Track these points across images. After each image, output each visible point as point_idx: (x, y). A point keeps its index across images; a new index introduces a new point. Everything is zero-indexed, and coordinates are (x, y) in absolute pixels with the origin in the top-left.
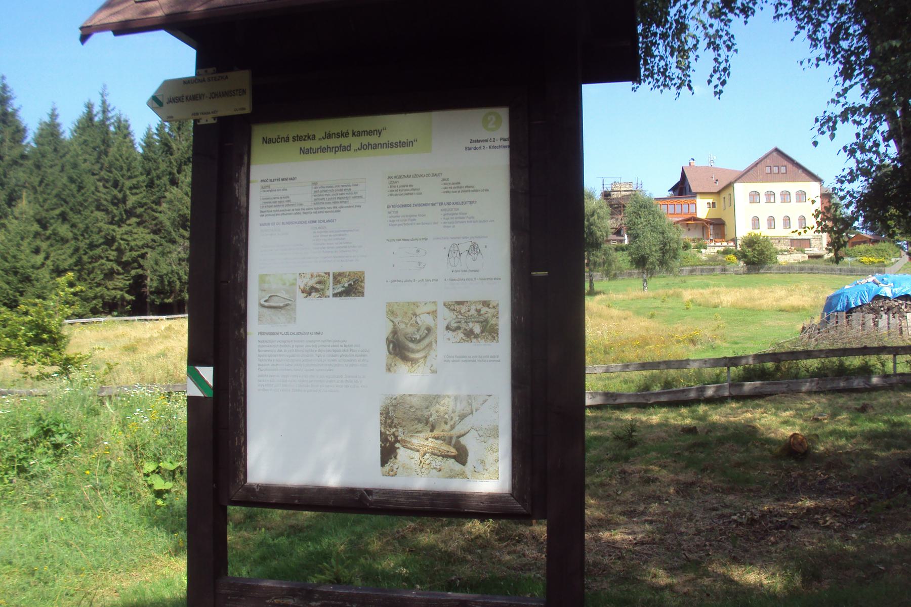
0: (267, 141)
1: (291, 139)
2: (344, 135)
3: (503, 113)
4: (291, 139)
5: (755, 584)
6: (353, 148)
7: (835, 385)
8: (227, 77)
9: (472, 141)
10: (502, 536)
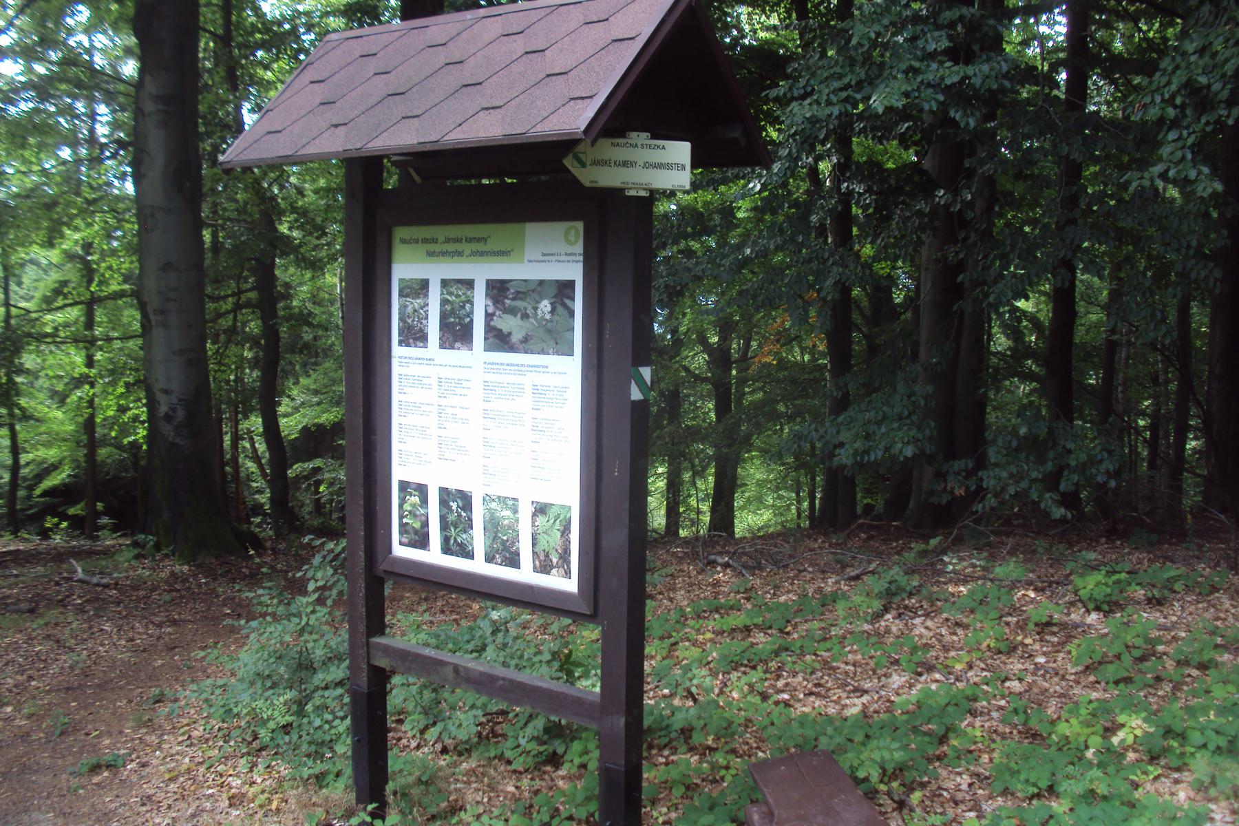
0: (403, 241)
3: (580, 225)
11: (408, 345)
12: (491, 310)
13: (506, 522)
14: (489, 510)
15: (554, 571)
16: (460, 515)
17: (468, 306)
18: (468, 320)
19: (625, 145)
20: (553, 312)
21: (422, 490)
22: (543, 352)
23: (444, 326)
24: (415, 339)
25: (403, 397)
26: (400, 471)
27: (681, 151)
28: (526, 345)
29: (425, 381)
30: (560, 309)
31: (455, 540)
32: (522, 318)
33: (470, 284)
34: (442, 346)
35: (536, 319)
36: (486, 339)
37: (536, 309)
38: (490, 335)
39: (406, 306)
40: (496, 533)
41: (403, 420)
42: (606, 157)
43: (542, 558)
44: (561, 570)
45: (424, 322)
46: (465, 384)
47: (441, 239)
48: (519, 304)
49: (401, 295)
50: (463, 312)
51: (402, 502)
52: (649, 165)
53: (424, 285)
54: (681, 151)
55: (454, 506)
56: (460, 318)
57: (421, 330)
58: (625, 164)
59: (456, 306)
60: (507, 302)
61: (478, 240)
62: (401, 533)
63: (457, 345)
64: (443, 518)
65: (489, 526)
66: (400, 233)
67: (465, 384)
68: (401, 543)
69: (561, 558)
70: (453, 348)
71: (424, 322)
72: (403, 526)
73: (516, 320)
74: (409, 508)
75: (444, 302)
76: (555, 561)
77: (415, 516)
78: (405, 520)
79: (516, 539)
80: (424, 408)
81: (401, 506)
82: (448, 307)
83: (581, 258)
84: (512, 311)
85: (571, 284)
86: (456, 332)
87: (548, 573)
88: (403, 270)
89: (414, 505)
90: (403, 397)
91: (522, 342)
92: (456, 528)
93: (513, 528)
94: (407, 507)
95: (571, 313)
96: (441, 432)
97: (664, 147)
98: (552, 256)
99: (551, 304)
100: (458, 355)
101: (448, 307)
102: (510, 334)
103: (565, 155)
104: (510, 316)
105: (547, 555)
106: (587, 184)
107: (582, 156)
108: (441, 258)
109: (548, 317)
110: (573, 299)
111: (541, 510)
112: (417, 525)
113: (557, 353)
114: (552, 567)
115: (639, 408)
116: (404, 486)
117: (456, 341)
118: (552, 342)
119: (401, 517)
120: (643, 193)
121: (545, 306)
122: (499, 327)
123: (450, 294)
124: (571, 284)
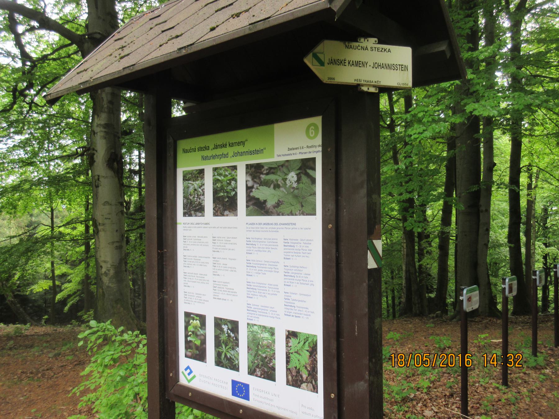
0: (185, 151)
1: (197, 150)
2: (224, 146)
3: (318, 121)
4: (197, 150)
5: (415, 318)
6: (210, 149)
7: (509, 303)
8: (355, 80)
9: (290, 149)
10: (136, 164)
11: (190, 215)
12: (250, 184)
13: (265, 342)
14: (252, 332)
15: (304, 385)
16: (229, 336)
17: (233, 183)
18: (234, 193)
19: (357, 48)
20: (299, 180)
21: (202, 318)
22: (291, 214)
23: (216, 199)
24: (196, 211)
25: (186, 253)
26: (184, 306)
27: (403, 55)
28: (277, 209)
29: (203, 240)
30: (304, 178)
31: (226, 355)
32: (274, 188)
33: (235, 168)
34: (215, 215)
35: (285, 188)
36: (247, 206)
37: (285, 180)
38: (251, 203)
39: (188, 187)
40: (257, 351)
41: (187, 270)
42: (342, 58)
43: (294, 374)
44: (310, 385)
45: (201, 197)
46: (233, 241)
47: (212, 147)
48: (272, 177)
49: (185, 179)
50: (230, 187)
51: (187, 324)
52: (377, 66)
53: (202, 172)
54: (403, 55)
55: (225, 328)
56: (227, 192)
57: (200, 204)
58: (358, 64)
59: (225, 183)
60: (263, 177)
61: (239, 144)
62: (186, 348)
63: (226, 212)
64: (217, 337)
65: (252, 346)
66: (183, 144)
67: (233, 241)
68: (186, 356)
69: (309, 375)
70: (223, 215)
71: (201, 197)
72: (187, 343)
73: (270, 193)
74: (192, 329)
75: (216, 181)
76: (305, 376)
77: (197, 335)
78: (189, 339)
79: (272, 357)
80: (203, 260)
81: (186, 328)
82: (219, 185)
83: (320, 149)
84: (266, 184)
85: (314, 159)
86: (225, 204)
87: (299, 387)
88: (185, 165)
89: (195, 327)
90: (186, 253)
91: (275, 207)
92: (226, 346)
93: (270, 346)
94: (190, 328)
95: (313, 181)
96: (217, 278)
97: (389, 51)
98: (298, 141)
99: (297, 175)
100: (227, 220)
101: (219, 185)
102: (265, 201)
103: (305, 54)
104: (265, 188)
105: (298, 372)
106: (325, 80)
107: (321, 56)
108: (212, 160)
109: (295, 185)
110: (314, 169)
111: (291, 335)
112: (198, 342)
113: (303, 214)
114: (302, 382)
115: (375, 274)
116: (188, 315)
117: (225, 210)
118: (299, 206)
119: (186, 336)
120: (372, 90)
121: (292, 177)
122: (257, 196)
123: (220, 175)
124: (314, 159)
